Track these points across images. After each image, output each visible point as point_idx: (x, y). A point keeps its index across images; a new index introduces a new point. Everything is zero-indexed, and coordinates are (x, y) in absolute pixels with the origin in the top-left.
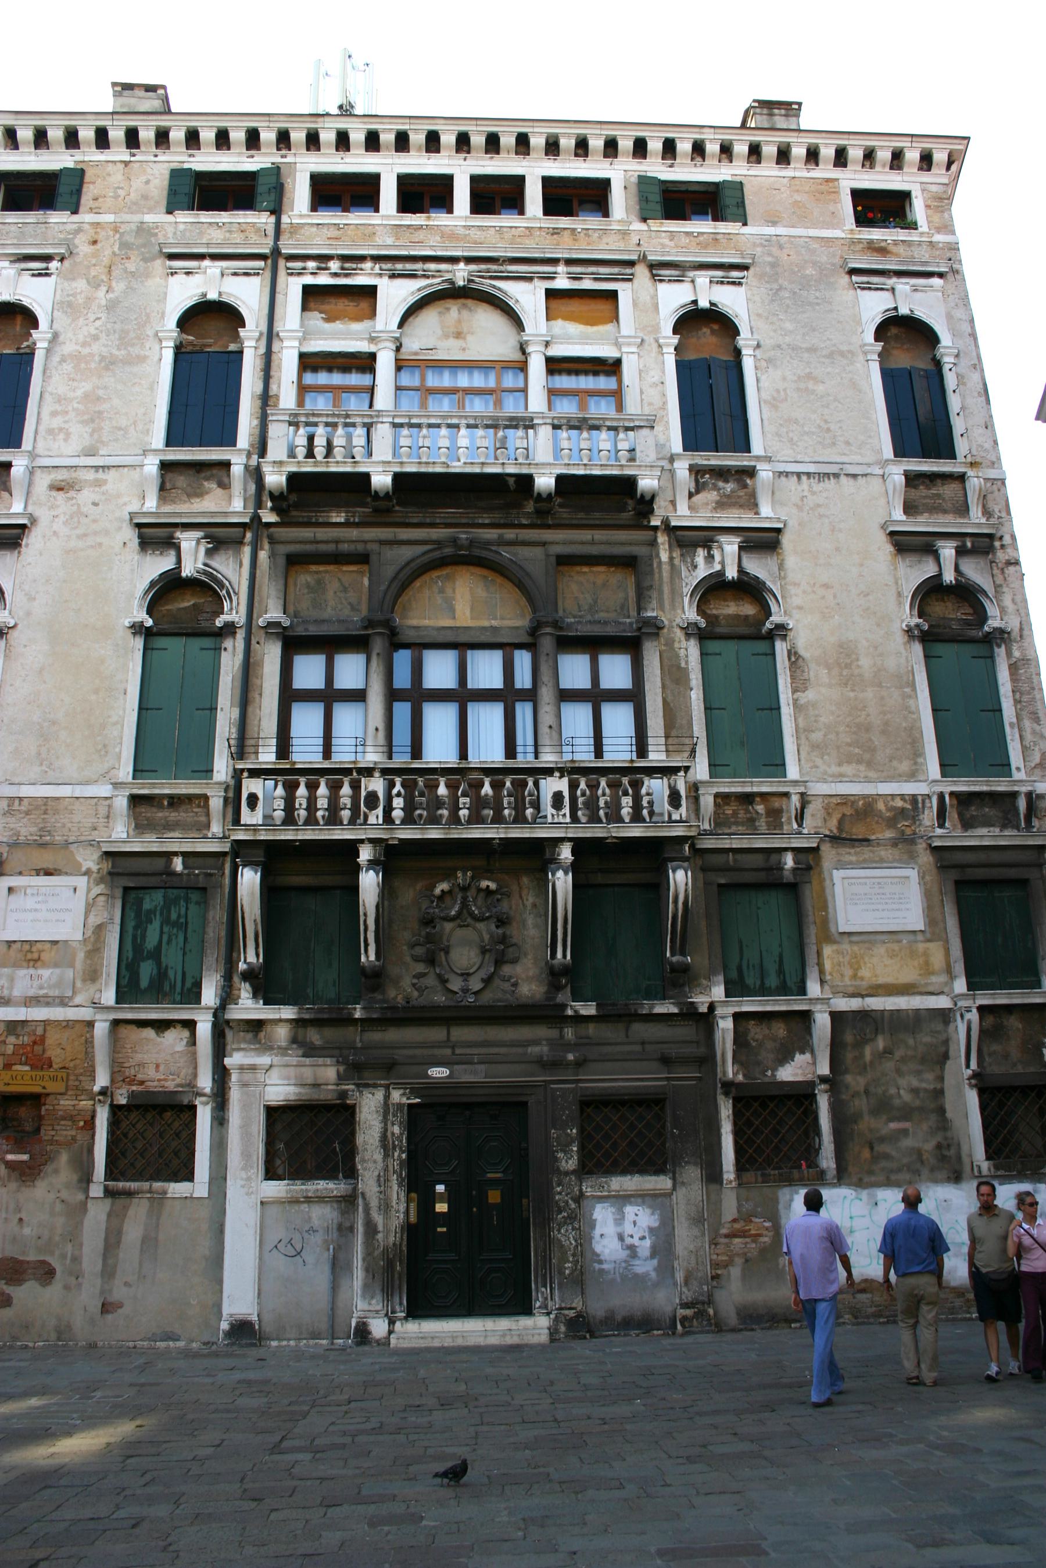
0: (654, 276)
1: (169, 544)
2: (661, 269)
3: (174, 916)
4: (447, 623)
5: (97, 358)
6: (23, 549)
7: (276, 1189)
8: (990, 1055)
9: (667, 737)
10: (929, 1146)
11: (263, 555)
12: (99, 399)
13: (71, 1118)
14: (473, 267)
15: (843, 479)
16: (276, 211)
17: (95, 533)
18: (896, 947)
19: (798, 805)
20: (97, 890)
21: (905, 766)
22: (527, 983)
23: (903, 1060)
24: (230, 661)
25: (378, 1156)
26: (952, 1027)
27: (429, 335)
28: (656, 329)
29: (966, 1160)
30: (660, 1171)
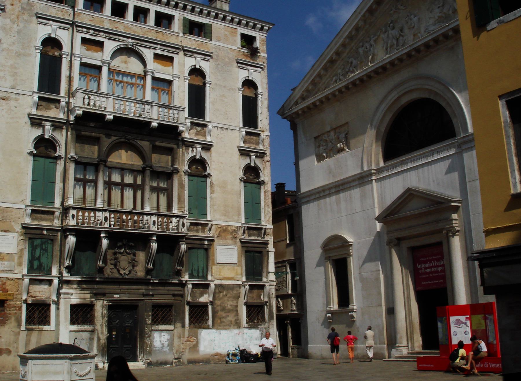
0: (185, 54)
2: (189, 52)
3: (44, 247)
4: (119, 161)
5: (15, 52)
7: (74, 327)
10: (233, 320)
11: (69, 133)
12: (16, 68)
13: (14, 307)
14: (133, 41)
16: (73, 7)
18: (230, 267)
20: (22, 238)
21: (236, 218)
22: (140, 272)
23: (230, 297)
24: (60, 166)
25: (101, 319)
26: (241, 289)
27: (119, 63)
28: (183, 72)
29: (241, 323)
30: (170, 324)
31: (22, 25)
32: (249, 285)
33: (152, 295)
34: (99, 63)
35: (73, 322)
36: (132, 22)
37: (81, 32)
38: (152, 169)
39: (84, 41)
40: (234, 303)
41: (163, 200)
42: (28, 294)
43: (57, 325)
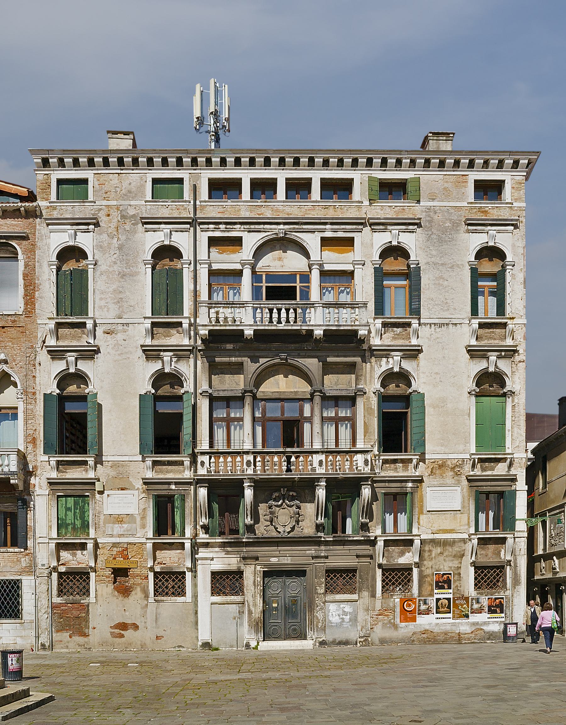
1: (159, 358)
2: (377, 225)
5: (117, 273)
6: (95, 360)
8: (480, 555)
9: (365, 436)
12: (120, 292)
14: (287, 227)
15: (451, 326)
17: (126, 353)
19: (416, 463)
22: (307, 528)
27: (273, 262)
31: (123, 238)
32: (478, 539)
33: (326, 557)
34: (239, 267)
35: (215, 591)
36: (284, 202)
37: (207, 230)
38: (324, 394)
39: (213, 242)
40: (455, 564)
41: (345, 432)
42: (154, 561)
43: (195, 596)
